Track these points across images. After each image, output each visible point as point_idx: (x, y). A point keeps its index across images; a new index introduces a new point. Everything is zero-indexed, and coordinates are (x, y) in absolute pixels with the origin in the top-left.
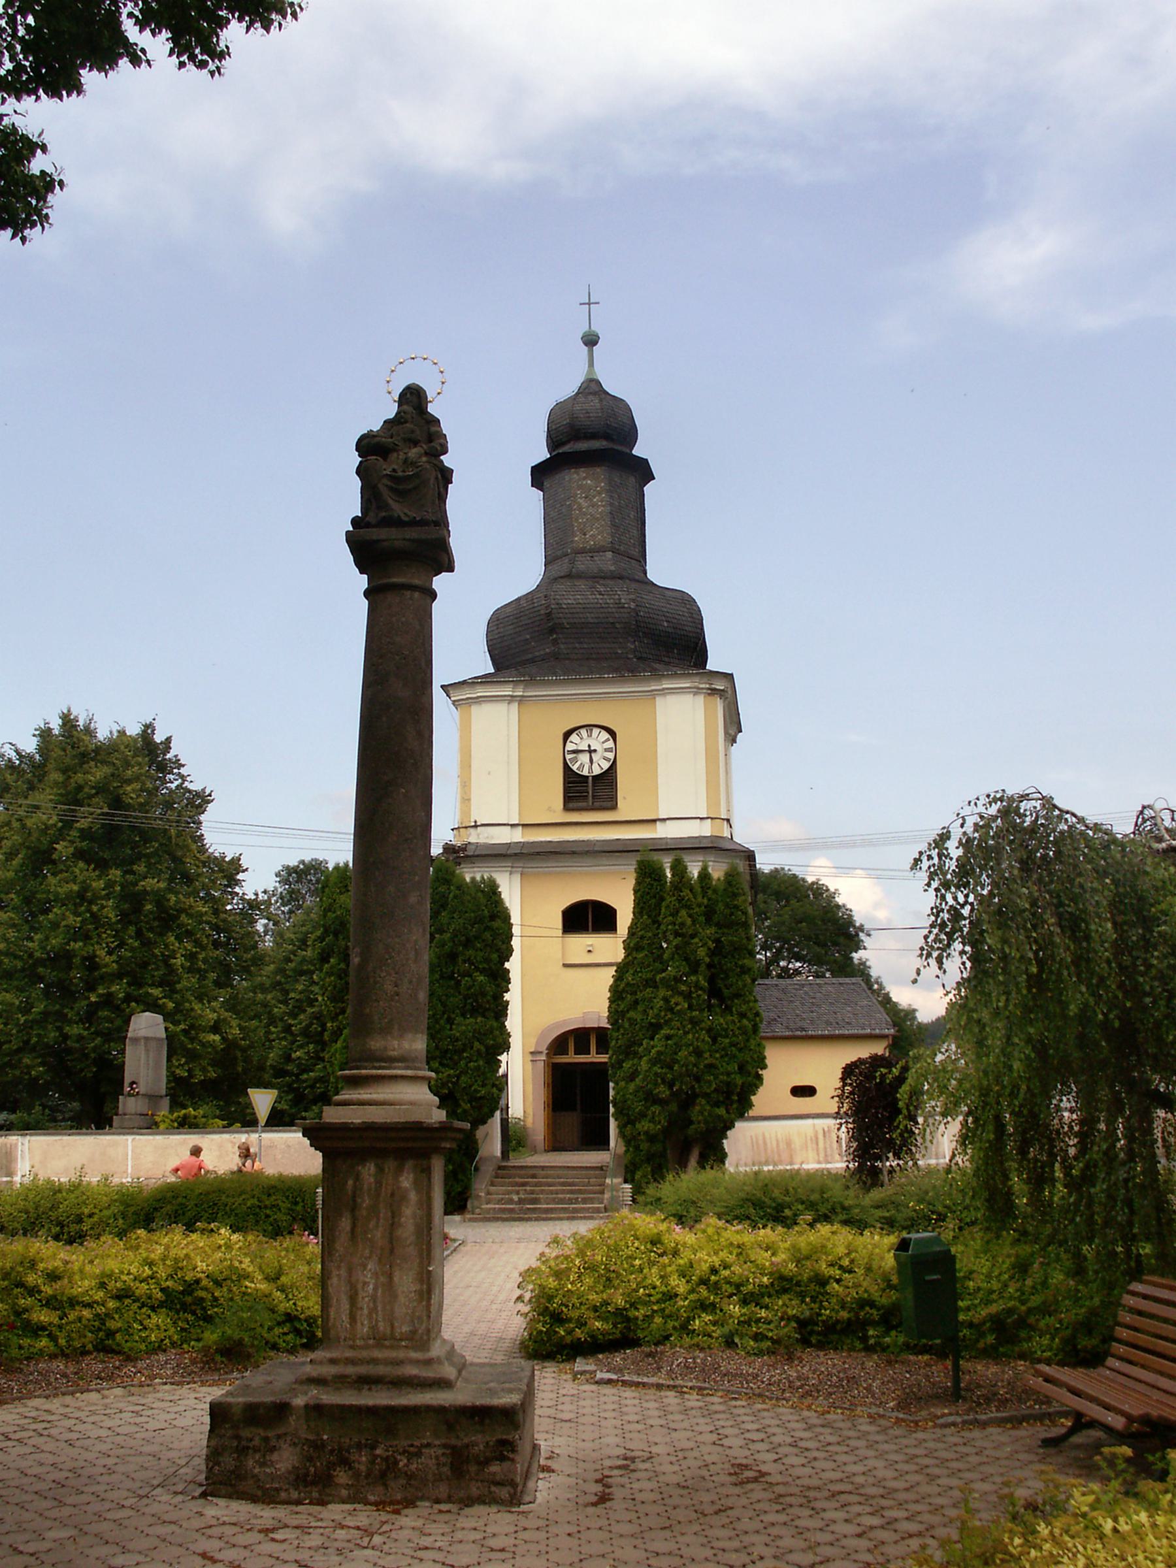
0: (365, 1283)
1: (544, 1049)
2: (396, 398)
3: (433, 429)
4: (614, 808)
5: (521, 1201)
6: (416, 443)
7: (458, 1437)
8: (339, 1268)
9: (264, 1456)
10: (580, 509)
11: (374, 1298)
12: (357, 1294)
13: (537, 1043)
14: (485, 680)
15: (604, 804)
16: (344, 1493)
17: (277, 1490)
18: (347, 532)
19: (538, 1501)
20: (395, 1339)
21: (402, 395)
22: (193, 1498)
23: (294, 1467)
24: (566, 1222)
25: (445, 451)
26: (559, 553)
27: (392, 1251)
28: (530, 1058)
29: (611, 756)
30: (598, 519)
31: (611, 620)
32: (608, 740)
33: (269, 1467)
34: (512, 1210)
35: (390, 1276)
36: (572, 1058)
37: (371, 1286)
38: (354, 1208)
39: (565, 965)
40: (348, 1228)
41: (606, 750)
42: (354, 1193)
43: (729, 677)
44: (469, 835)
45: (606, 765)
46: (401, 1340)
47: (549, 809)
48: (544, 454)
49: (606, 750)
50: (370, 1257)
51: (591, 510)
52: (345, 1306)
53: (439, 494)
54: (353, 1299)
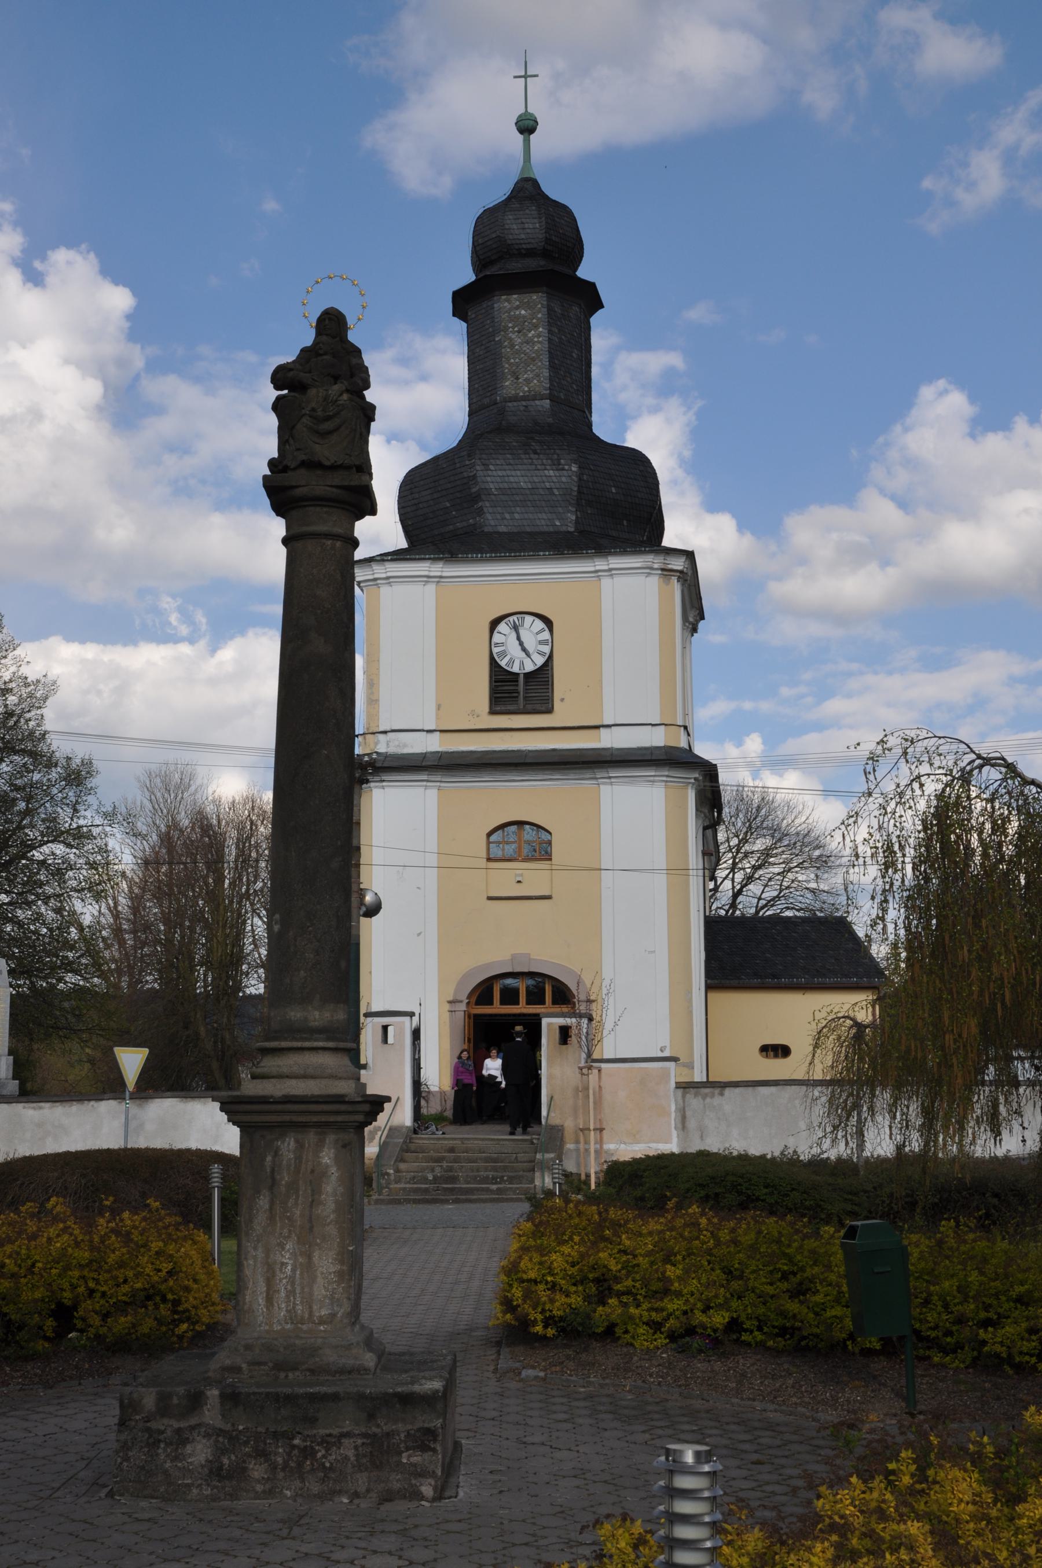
0: (283, 1264)
1: (463, 996)
2: (314, 324)
3: (354, 361)
4: (550, 711)
5: (436, 1179)
6: (336, 379)
7: (378, 1426)
8: (255, 1248)
9: (177, 1449)
10: (512, 346)
11: (292, 1280)
12: (274, 1275)
13: (456, 991)
14: (397, 556)
15: (538, 707)
16: (259, 1488)
17: (188, 1485)
18: (265, 477)
19: (459, 1497)
20: (313, 1322)
21: (320, 321)
22: (100, 1499)
23: (207, 1461)
24: (489, 1205)
25: (367, 386)
26: (486, 401)
27: (311, 1229)
28: (447, 1007)
29: (546, 649)
30: (534, 360)
31: (548, 485)
32: (542, 630)
33: (181, 1461)
34: (426, 1191)
35: (310, 1257)
36: (497, 1008)
37: (289, 1268)
38: (273, 1184)
39: (490, 898)
40: (267, 1206)
41: (541, 642)
42: (273, 1171)
43: (690, 555)
44: (377, 743)
45: (540, 661)
46: (320, 1324)
47: (473, 713)
48: (466, 276)
49: (541, 642)
50: (289, 1237)
51: (526, 348)
52: (262, 1287)
53: (361, 434)
54: (269, 1282)
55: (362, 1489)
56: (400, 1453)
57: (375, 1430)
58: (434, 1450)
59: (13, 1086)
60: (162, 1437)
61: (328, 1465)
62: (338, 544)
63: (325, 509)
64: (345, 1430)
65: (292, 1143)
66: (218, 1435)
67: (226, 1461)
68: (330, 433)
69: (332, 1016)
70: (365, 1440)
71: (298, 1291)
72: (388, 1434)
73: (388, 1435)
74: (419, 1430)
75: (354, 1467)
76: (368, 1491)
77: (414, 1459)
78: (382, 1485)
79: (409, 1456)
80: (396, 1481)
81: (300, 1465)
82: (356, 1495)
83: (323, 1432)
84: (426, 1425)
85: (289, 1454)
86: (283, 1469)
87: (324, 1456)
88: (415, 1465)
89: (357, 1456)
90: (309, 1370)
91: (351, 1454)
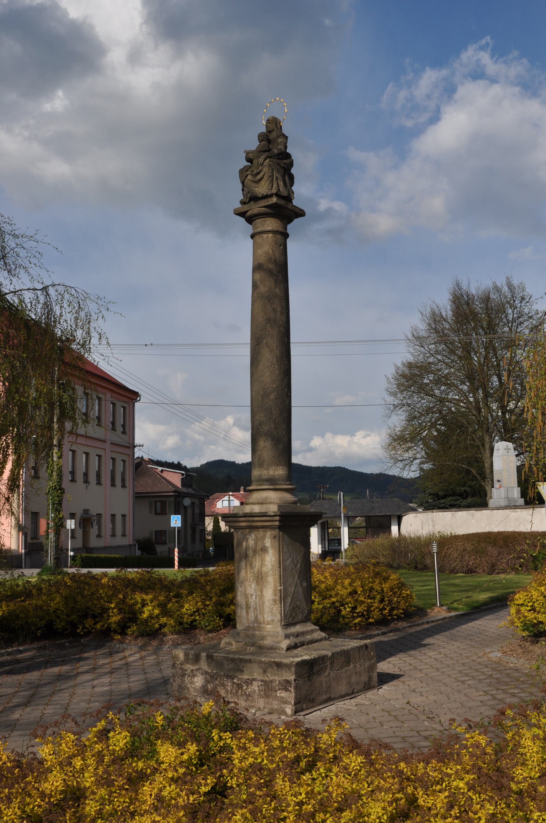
7: (268, 677)
55: (262, 707)
56: (276, 691)
57: (267, 679)
58: (290, 691)
59: (522, 501)
60: (186, 673)
61: (248, 693)
62: (270, 235)
63: (263, 219)
64: (254, 677)
65: (253, 536)
66: (206, 674)
67: (209, 687)
68: (260, 180)
69: (274, 473)
70: (262, 683)
71: (258, 608)
72: (271, 681)
73: (271, 682)
74: (284, 680)
75: (258, 695)
76: (264, 708)
77: (282, 695)
78: (270, 706)
79: (280, 693)
80: (275, 705)
81: (237, 692)
82: (259, 709)
83: (246, 677)
84: (287, 679)
85: (232, 686)
86: (231, 693)
87: (246, 689)
88: (282, 698)
89: (259, 690)
90: (258, 646)
91: (257, 689)
